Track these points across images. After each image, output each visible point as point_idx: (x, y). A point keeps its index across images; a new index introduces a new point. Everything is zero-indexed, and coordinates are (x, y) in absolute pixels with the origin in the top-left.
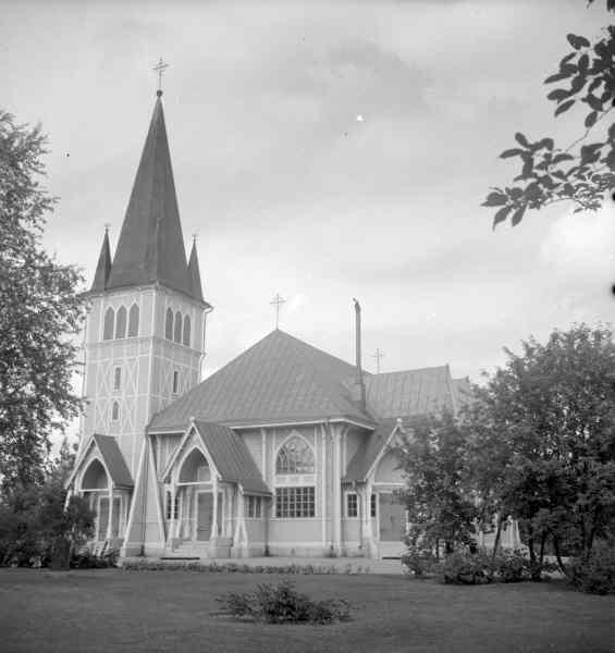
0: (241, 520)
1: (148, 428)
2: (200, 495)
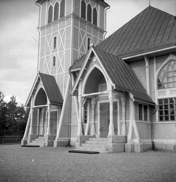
0: (132, 122)
1: (70, 68)
2: (101, 104)
